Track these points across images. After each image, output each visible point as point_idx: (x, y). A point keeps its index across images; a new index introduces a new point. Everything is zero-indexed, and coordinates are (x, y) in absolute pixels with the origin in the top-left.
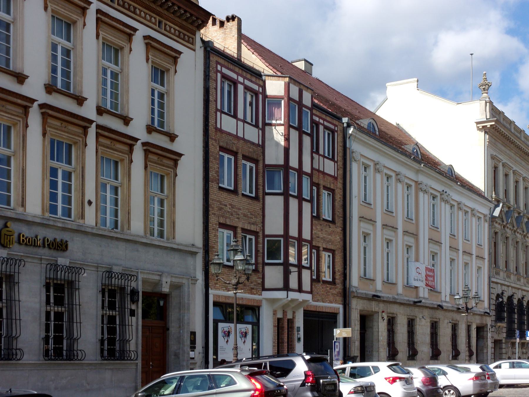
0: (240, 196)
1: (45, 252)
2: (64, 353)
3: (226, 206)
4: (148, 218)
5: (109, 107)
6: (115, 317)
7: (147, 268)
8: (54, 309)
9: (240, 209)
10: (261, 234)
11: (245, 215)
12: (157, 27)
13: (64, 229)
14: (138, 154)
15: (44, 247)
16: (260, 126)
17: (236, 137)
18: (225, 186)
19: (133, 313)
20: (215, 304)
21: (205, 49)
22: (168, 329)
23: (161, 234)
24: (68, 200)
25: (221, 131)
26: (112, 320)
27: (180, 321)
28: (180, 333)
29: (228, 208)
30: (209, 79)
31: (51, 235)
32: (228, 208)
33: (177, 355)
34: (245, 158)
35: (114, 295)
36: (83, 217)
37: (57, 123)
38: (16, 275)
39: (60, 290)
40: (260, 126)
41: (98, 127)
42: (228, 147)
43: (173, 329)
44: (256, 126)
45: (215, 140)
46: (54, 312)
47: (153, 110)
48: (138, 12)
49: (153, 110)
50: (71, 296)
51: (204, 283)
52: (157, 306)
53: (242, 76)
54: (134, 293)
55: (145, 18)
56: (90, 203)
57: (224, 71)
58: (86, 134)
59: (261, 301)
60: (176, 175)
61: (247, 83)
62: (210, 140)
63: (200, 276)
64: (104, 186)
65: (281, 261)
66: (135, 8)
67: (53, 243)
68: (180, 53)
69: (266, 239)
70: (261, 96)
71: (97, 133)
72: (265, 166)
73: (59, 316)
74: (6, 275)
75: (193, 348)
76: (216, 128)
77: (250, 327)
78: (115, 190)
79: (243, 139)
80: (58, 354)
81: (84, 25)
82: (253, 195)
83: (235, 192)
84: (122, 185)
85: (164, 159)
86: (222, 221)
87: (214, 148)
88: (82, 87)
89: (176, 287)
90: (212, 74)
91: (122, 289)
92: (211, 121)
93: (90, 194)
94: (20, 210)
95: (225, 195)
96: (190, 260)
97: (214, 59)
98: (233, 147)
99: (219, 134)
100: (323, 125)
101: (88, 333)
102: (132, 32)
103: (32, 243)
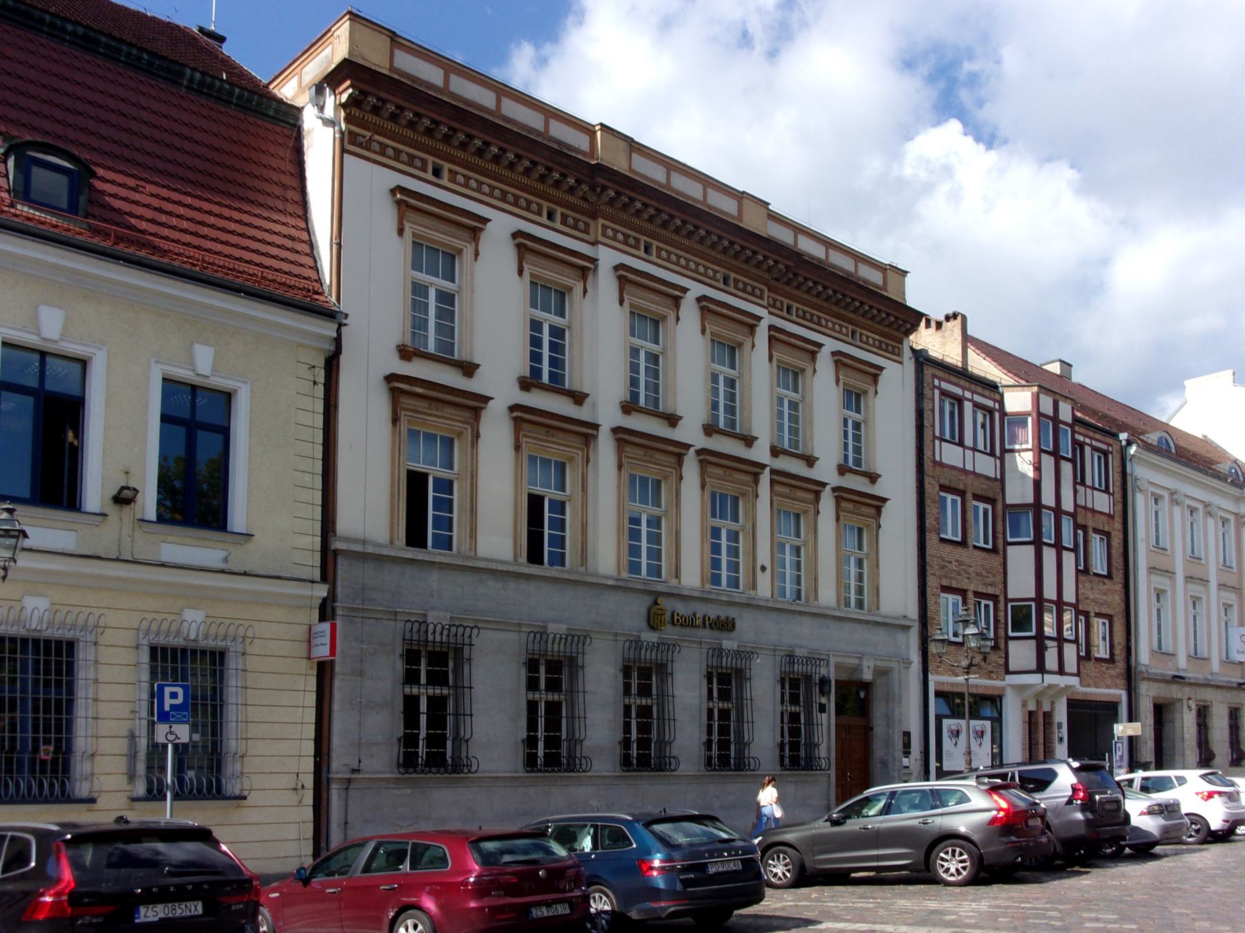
1: (706, 634)
4: (842, 585)
7: (840, 650)
8: (718, 705)
10: (1002, 599)
11: (977, 574)
14: (605, 449)
15: (704, 626)
16: (998, 453)
17: (964, 471)
18: (949, 536)
19: (822, 709)
20: (938, 694)
22: (872, 729)
23: (860, 604)
24: (734, 567)
25: (941, 464)
27: (889, 718)
29: (954, 566)
31: (713, 612)
32: (954, 566)
33: (884, 764)
35: (797, 685)
36: (754, 587)
37: (422, 405)
39: (726, 681)
40: (998, 453)
41: (773, 472)
43: (879, 729)
44: (992, 454)
52: (856, 699)
53: (969, 390)
54: (824, 682)
56: (763, 568)
57: (944, 385)
59: (1003, 689)
60: (476, 436)
61: (977, 398)
66: (577, 221)
69: (1009, 605)
70: (997, 415)
72: (1006, 506)
75: (907, 753)
76: (934, 461)
78: (797, 551)
79: (974, 473)
81: (477, 254)
82: (990, 546)
83: (963, 543)
87: (931, 488)
89: (883, 673)
90: (927, 392)
91: (808, 678)
93: (764, 557)
95: (949, 548)
96: (900, 636)
97: (928, 371)
99: (938, 468)
100: (939, 388)
101: (763, 733)
103: (688, 623)
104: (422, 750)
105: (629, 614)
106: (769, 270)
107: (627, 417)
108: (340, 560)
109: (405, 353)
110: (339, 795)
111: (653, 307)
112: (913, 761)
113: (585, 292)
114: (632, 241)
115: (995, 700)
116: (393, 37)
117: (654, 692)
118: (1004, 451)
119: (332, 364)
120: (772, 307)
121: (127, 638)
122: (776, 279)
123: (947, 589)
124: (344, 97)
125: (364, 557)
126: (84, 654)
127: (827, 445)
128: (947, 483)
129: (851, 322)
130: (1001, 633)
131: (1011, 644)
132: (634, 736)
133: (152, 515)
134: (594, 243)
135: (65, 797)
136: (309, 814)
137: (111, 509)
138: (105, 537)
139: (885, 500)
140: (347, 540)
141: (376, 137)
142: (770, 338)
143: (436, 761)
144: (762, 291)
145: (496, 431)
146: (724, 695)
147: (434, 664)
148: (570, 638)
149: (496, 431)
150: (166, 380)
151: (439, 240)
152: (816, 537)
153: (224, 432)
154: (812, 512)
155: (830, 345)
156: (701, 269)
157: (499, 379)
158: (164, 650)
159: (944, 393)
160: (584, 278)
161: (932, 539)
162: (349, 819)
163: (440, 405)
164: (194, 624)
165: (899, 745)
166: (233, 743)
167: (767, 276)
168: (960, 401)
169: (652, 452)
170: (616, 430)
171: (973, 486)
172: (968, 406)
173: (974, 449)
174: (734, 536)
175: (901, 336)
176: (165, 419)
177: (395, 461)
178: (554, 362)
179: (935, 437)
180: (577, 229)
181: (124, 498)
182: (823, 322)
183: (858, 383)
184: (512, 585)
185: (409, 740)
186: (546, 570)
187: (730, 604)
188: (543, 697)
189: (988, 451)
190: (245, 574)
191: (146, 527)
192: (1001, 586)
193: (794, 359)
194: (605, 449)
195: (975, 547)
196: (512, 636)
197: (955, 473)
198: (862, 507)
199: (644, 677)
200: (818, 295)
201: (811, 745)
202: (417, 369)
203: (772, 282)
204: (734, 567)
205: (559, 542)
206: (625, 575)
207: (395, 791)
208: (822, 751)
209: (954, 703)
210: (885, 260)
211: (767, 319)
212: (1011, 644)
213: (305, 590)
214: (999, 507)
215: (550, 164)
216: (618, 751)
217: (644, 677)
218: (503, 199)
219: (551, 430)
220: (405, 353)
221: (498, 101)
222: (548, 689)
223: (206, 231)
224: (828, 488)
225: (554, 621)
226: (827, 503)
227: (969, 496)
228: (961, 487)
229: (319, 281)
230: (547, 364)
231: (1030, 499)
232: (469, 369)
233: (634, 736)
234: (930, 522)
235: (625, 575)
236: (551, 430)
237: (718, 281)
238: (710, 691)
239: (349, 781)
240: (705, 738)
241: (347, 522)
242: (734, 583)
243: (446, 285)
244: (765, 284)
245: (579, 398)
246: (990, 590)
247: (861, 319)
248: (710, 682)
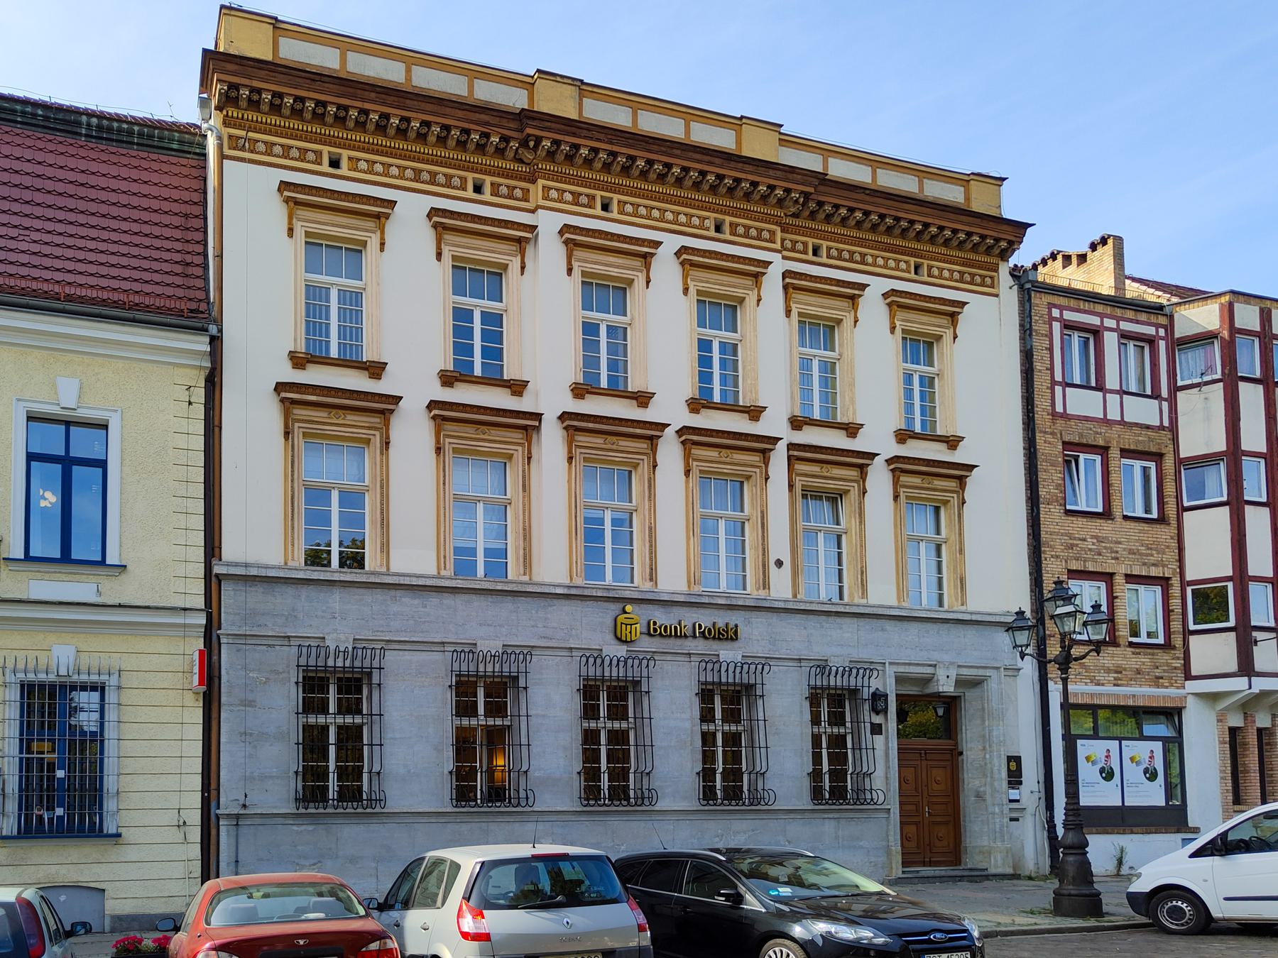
0: (1119, 520)
1: (699, 646)
2: (632, 794)
3: (1084, 540)
5: (918, 429)
6: (844, 737)
9: (1120, 543)
10: (1176, 581)
11: (1131, 552)
15: (694, 636)
16: (1165, 393)
18: (1082, 507)
19: (876, 729)
21: (1021, 287)
22: (961, 753)
25: (1065, 416)
27: (985, 740)
28: (984, 758)
30: (1030, 335)
31: (706, 619)
34: (1126, 453)
35: (834, 701)
36: (766, 585)
37: (916, 480)
38: (644, 681)
39: (729, 700)
40: (1165, 393)
42: (1084, 441)
44: (1156, 395)
45: (1053, 434)
46: (723, 733)
48: (870, 260)
50: (638, 703)
51: (1037, 674)
52: (933, 720)
53: (1111, 317)
54: (878, 700)
55: (885, 266)
56: (779, 563)
60: (387, 444)
62: (1038, 435)
65: (1232, 623)
66: (863, 255)
67: (710, 631)
69: (1189, 590)
70: (1162, 344)
71: (789, 458)
72: (1181, 462)
74: (510, 677)
76: (1054, 414)
79: (1122, 422)
80: (838, 793)
81: (955, 337)
82: (1155, 515)
83: (1107, 514)
85: (934, 478)
86: (1075, 566)
87: (1049, 448)
88: (756, 393)
90: (1039, 326)
91: (854, 692)
94: (648, 586)
95: (1081, 522)
97: (1040, 301)
99: (1060, 422)
100: (1061, 320)
102: (857, 292)
104: (605, 782)
106: (780, 202)
107: (448, 389)
108: (224, 585)
109: (447, 379)
110: (228, 835)
111: (614, 272)
113: (523, 268)
114: (584, 200)
115: (1172, 714)
116: (275, 22)
117: (631, 714)
118: (1175, 389)
119: (213, 382)
122: (795, 215)
128: (1076, 439)
130: (1176, 626)
131: (1193, 640)
132: (825, 767)
136: (196, 851)
139: (971, 467)
141: (251, 134)
142: (786, 287)
143: (619, 793)
144: (772, 233)
145: (412, 433)
147: (337, 693)
148: (854, 671)
149: (412, 433)
152: (862, 520)
156: (682, 218)
159: (1068, 326)
161: (1051, 517)
162: (241, 856)
163: (340, 412)
167: (780, 213)
168: (1096, 333)
169: (614, 438)
170: (564, 416)
171: (1118, 440)
172: (1110, 340)
175: (994, 260)
178: (612, 366)
179: (1054, 383)
182: (870, 260)
184: (434, 600)
185: (707, 774)
188: (604, 724)
189: (1149, 392)
190: (120, 606)
191: (13, 566)
192: (1175, 566)
194: (552, 439)
195: (1126, 518)
196: (437, 656)
197: (1089, 425)
199: (610, 697)
200: (859, 224)
202: (316, 376)
203: (790, 220)
206: (579, 581)
207: (295, 828)
208: (878, 781)
210: (966, 167)
211: (778, 265)
212: (1193, 640)
214: (1169, 463)
215: (466, 125)
216: (806, 783)
217: (610, 697)
218: (417, 179)
219: (483, 424)
220: (298, 361)
221: (408, 71)
222: (611, 717)
224: (670, 432)
225: (482, 638)
227: (1114, 453)
228: (1101, 443)
230: (477, 348)
231: (1219, 443)
232: (376, 370)
233: (825, 767)
237: (707, 229)
239: (238, 816)
241: (233, 549)
243: (729, 336)
244: (776, 224)
246: (1154, 572)
247: (929, 247)
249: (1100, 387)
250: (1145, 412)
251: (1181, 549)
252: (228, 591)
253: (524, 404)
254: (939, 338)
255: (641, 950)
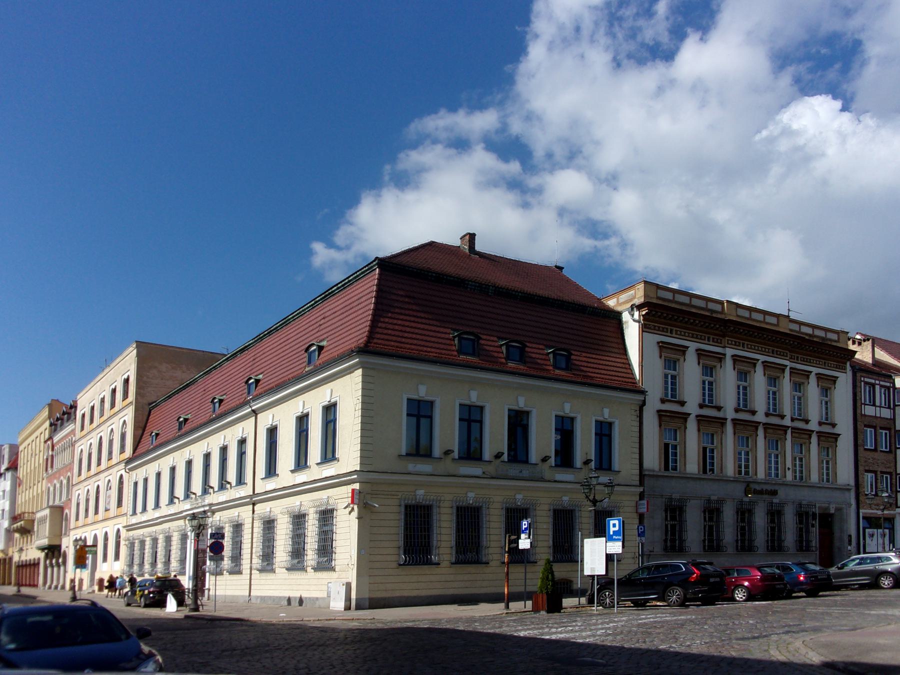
4: (821, 474)
7: (820, 500)
8: (669, 523)
12: (706, 342)
13: (775, 484)
14: (729, 428)
17: (876, 417)
18: (869, 447)
19: (813, 526)
20: (863, 518)
23: (828, 480)
24: (777, 469)
25: (865, 415)
26: (711, 527)
29: (871, 461)
31: (769, 488)
32: (871, 461)
33: (839, 549)
34: (881, 428)
35: (803, 515)
37: (667, 419)
39: (775, 515)
41: (793, 428)
43: (837, 534)
44: (889, 407)
47: (739, 399)
49: (739, 399)
52: (827, 521)
54: (814, 514)
57: (866, 380)
58: (786, 434)
59: (895, 515)
60: (686, 428)
61: (882, 383)
63: (853, 502)
64: (795, 458)
68: (688, 347)
72: (896, 431)
73: (711, 527)
75: (850, 544)
77: (887, 531)
78: (801, 460)
83: (875, 450)
84: (805, 456)
86: (867, 468)
87: (860, 426)
89: (838, 510)
90: (858, 384)
92: (858, 411)
93: (789, 464)
95: (868, 453)
96: (847, 493)
98: (874, 424)
101: (790, 538)
103: (761, 492)
105: (738, 491)
109: (663, 401)
111: (673, 356)
112: (852, 548)
118: (895, 406)
120: (791, 359)
121: (546, 507)
123: (867, 471)
124: (644, 313)
125: (653, 476)
126: (435, 511)
127: (814, 413)
129: (824, 359)
133: (457, 457)
134: (724, 347)
135: (38, 564)
137: (583, 467)
138: (490, 469)
140: (649, 470)
146: (673, 518)
147: (675, 511)
149: (692, 425)
150: (460, 405)
151: (671, 356)
153: (481, 422)
154: (719, 432)
155: (815, 370)
157: (692, 408)
158: (410, 506)
159: (866, 383)
160: (721, 362)
161: (861, 449)
164: (471, 497)
165: (846, 540)
166: (435, 542)
168: (873, 385)
170: (733, 420)
172: (877, 387)
173: (880, 407)
174: (776, 457)
176: (460, 420)
177: (699, 444)
180: (717, 342)
181: (587, 462)
183: (827, 384)
186: (671, 473)
187: (775, 484)
193: (800, 380)
194: (729, 428)
198: (829, 439)
199: (744, 513)
201: (808, 542)
204: (777, 469)
205: (712, 464)
209: (873, 522)
213: (633, 489)
214: (893, 431)
217: (744, 513)
220: (663, 401)
223: (406, 335)
226: (814, 439)
229: (635, 379)
230: (709, 399)
234: (860, 442)
235: (737, 476)
236: (711, 424)
238: (666, 516)
240: (664, 538)
242: (777, 475)
245: (719, 408)
246: (888, 470)
248: (705, 514)
249: (874, 405)
250: (886, 413)
251: (896, 462)
252: (646, 479)
253: (720, 414)
254: (803, 383)
255: (174, 595)
